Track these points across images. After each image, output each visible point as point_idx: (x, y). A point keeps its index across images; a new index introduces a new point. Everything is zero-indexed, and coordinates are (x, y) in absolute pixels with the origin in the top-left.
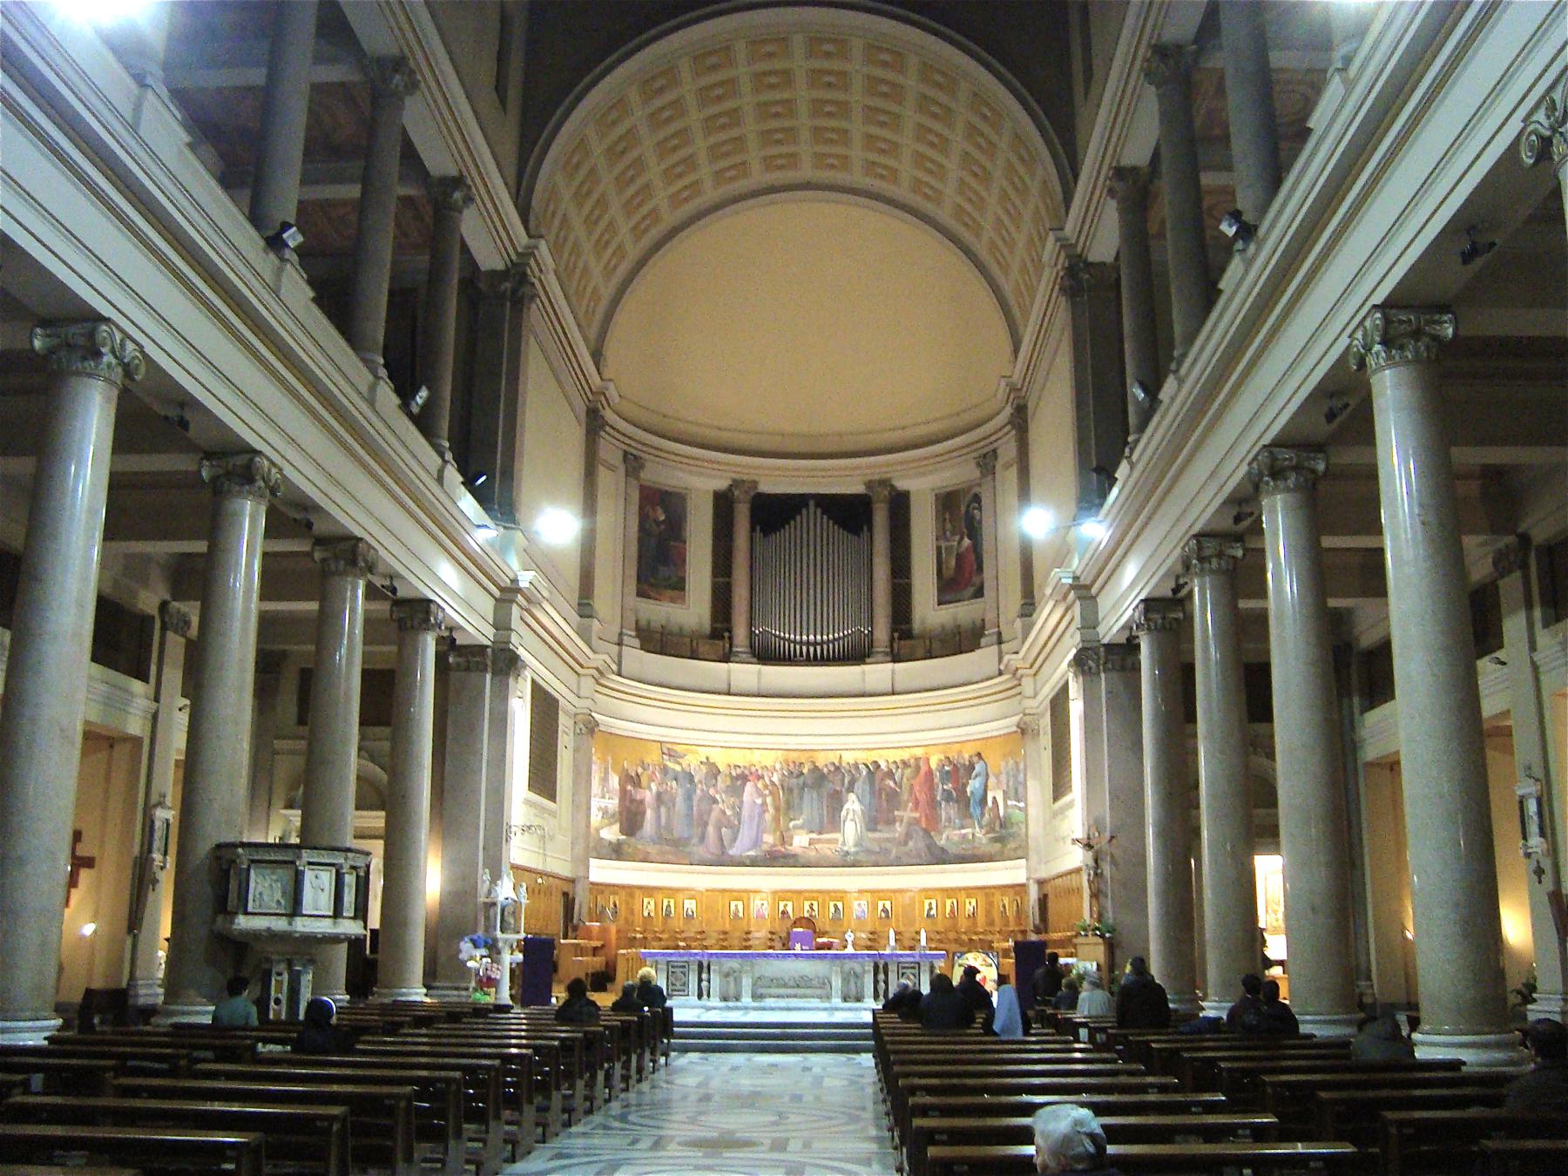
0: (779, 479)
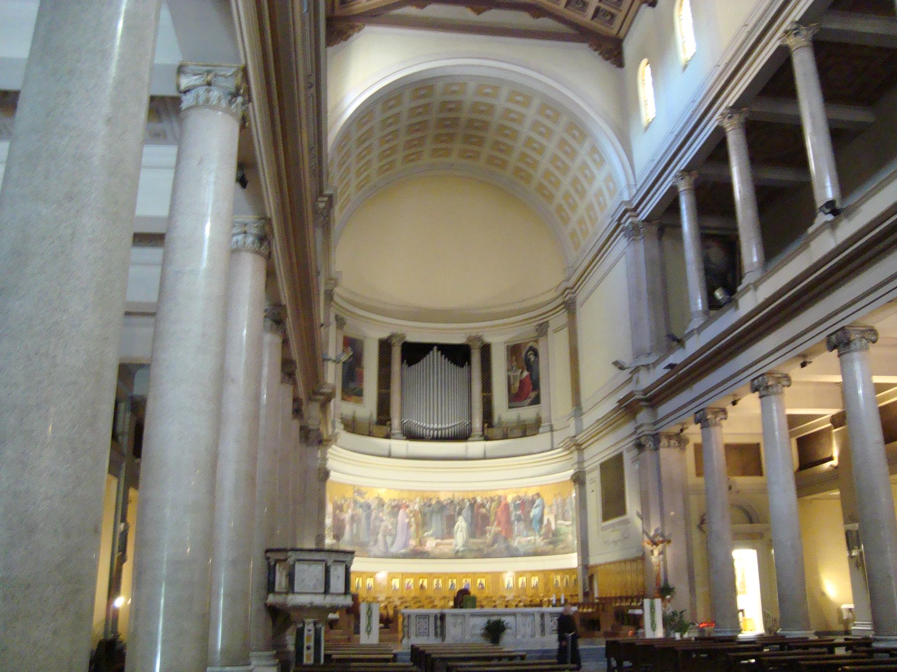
0: (417, 334)
